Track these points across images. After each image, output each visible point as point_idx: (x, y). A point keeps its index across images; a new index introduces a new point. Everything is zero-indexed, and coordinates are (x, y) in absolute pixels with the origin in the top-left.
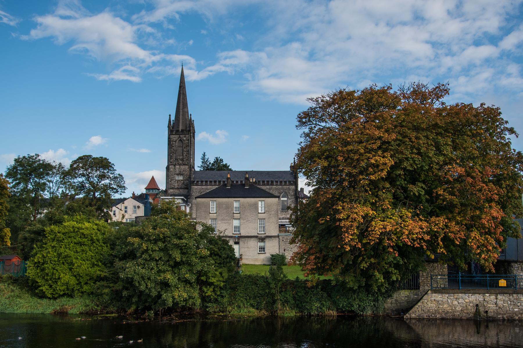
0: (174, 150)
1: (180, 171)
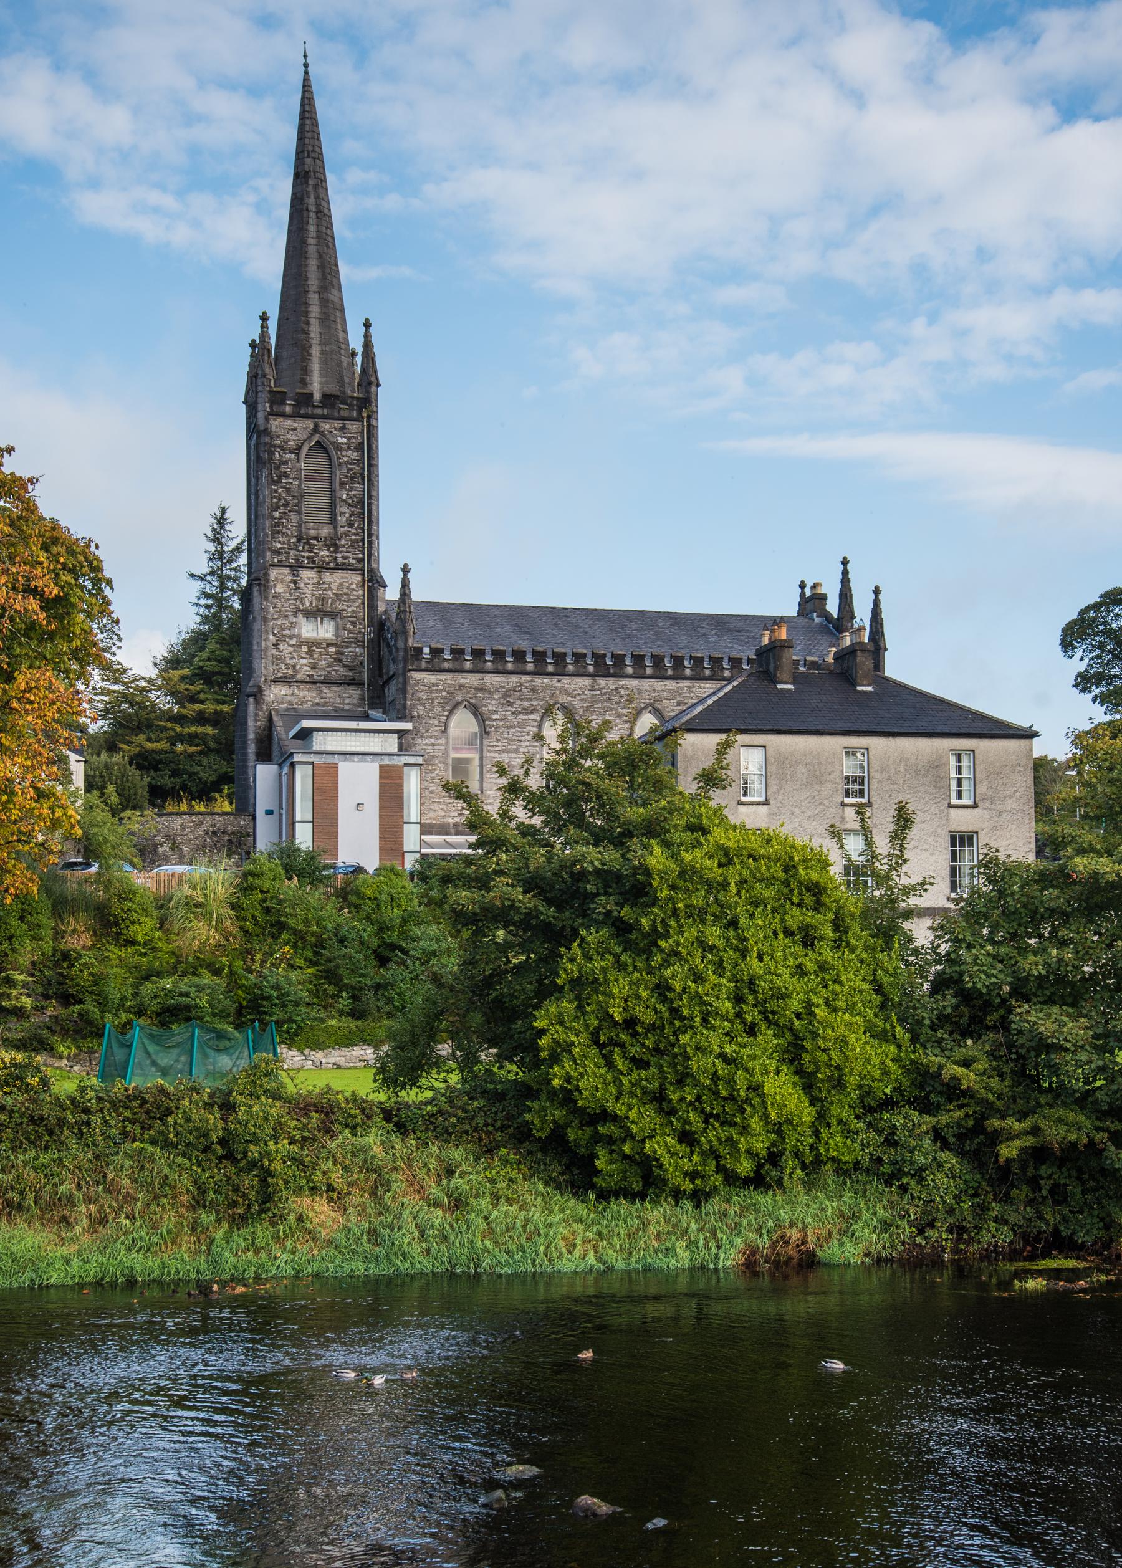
0: (288, 490)
1: (323, 599)
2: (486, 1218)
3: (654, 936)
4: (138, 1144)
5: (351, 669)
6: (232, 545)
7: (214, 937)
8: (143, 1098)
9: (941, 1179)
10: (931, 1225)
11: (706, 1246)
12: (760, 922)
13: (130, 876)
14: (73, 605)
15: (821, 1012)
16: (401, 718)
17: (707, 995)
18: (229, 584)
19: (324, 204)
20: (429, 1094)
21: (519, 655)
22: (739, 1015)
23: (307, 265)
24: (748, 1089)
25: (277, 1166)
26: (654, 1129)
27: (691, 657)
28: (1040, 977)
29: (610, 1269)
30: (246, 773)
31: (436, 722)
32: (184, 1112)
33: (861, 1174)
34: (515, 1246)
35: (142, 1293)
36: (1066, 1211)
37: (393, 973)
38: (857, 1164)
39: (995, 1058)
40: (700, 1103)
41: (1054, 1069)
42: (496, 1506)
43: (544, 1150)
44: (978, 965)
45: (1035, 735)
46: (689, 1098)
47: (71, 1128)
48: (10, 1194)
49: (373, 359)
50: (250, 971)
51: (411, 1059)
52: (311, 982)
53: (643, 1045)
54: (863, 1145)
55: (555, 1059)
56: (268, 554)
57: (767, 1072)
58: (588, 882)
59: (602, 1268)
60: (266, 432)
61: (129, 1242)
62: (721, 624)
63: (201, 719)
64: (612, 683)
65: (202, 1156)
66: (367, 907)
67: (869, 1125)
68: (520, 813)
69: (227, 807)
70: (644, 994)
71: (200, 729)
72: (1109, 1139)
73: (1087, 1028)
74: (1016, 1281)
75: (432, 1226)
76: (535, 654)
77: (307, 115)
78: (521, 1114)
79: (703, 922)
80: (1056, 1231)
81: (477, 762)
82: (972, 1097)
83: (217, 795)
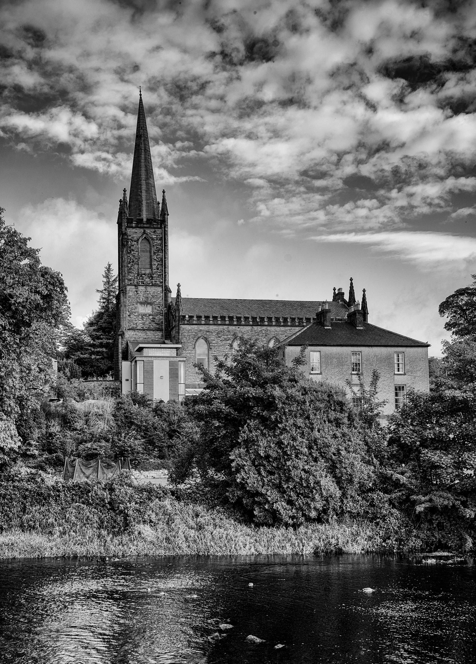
0: (134, 256)
2: (212, 533)
3: (277, 421)
4: (78, 504)
5: (158, 324)
6: (113, 279)
7: (106, 428)
8: (80, 486)
9: (393, 520)
10: (389, 538)
11: (299, 546)
12: (319, 417)
13: (74, 404)
14: (53, 298)
15: (343, 453)
16: (177, 343)
17: (297, 446)
18: (112, 294)
19: (147, 147)
20: (189, 486)
21: (223, 318)
22: (310, 454)
23: (141, 170)
24: (314, 483)
25: (131, 512)
26: (277, 499)
27: (290, 318)
28: (431, 439)
29: (260, 554)
30: (118, 365)
31: (191, 345)
32: (95, 492)
33: (360, 518)
34: (223, 545)
35: (79, 560)
36: (444, 533)
37: (175, 441)
38: (358, 514)
39: (414, 472)
40: (295, 489)
41: (438, 476)
42: (216, 638)
43: (234, 508)
44: (406, 434)
45: (429, 346)
46: (291, 487)
47: (53, 497)
48: (30, 523)
49: (166, 205)
50: (120, 440)
51: (181, 472)
52: (143, 445)
53: (272, 466)
54: (361, 506)
55: (238, 471)
56: (126, 280)
57: (322, 477)
58: (250, 402)
59: (257, 554)
60: (126, 234)
61: (74, 541)
62: (302, 305)
63: (101, 345)
64: (259, 328)
65: (102, 509)
66: (165, 416)
67: (363, 498)
68: (224, 375)
69: (111, 379)
70: (273, 446)
71: (101, 350)
72: (461, 504)
73: (451, 459)
74: (423, 560)
75: (190, 536)
76: (229, 317)
77: (141, 113)
78: (225, 493)
79: (296, 417)
80: (440, 541)
81: (207, 360)
82: (405, 487)
83: (107, 375)
